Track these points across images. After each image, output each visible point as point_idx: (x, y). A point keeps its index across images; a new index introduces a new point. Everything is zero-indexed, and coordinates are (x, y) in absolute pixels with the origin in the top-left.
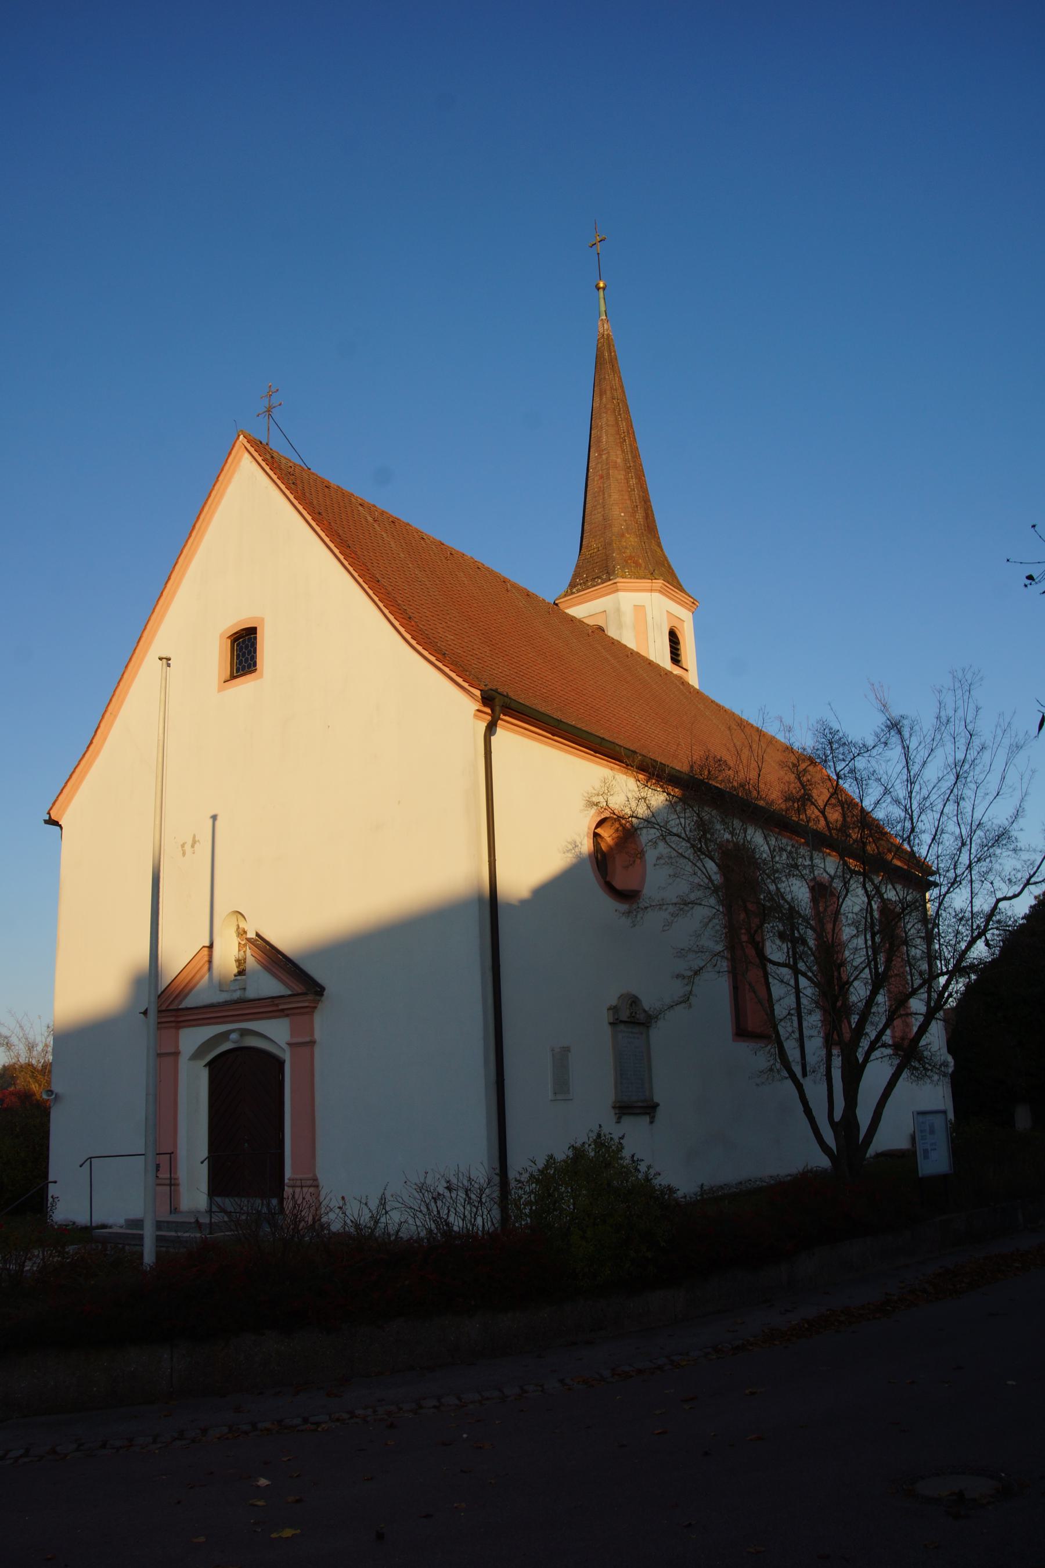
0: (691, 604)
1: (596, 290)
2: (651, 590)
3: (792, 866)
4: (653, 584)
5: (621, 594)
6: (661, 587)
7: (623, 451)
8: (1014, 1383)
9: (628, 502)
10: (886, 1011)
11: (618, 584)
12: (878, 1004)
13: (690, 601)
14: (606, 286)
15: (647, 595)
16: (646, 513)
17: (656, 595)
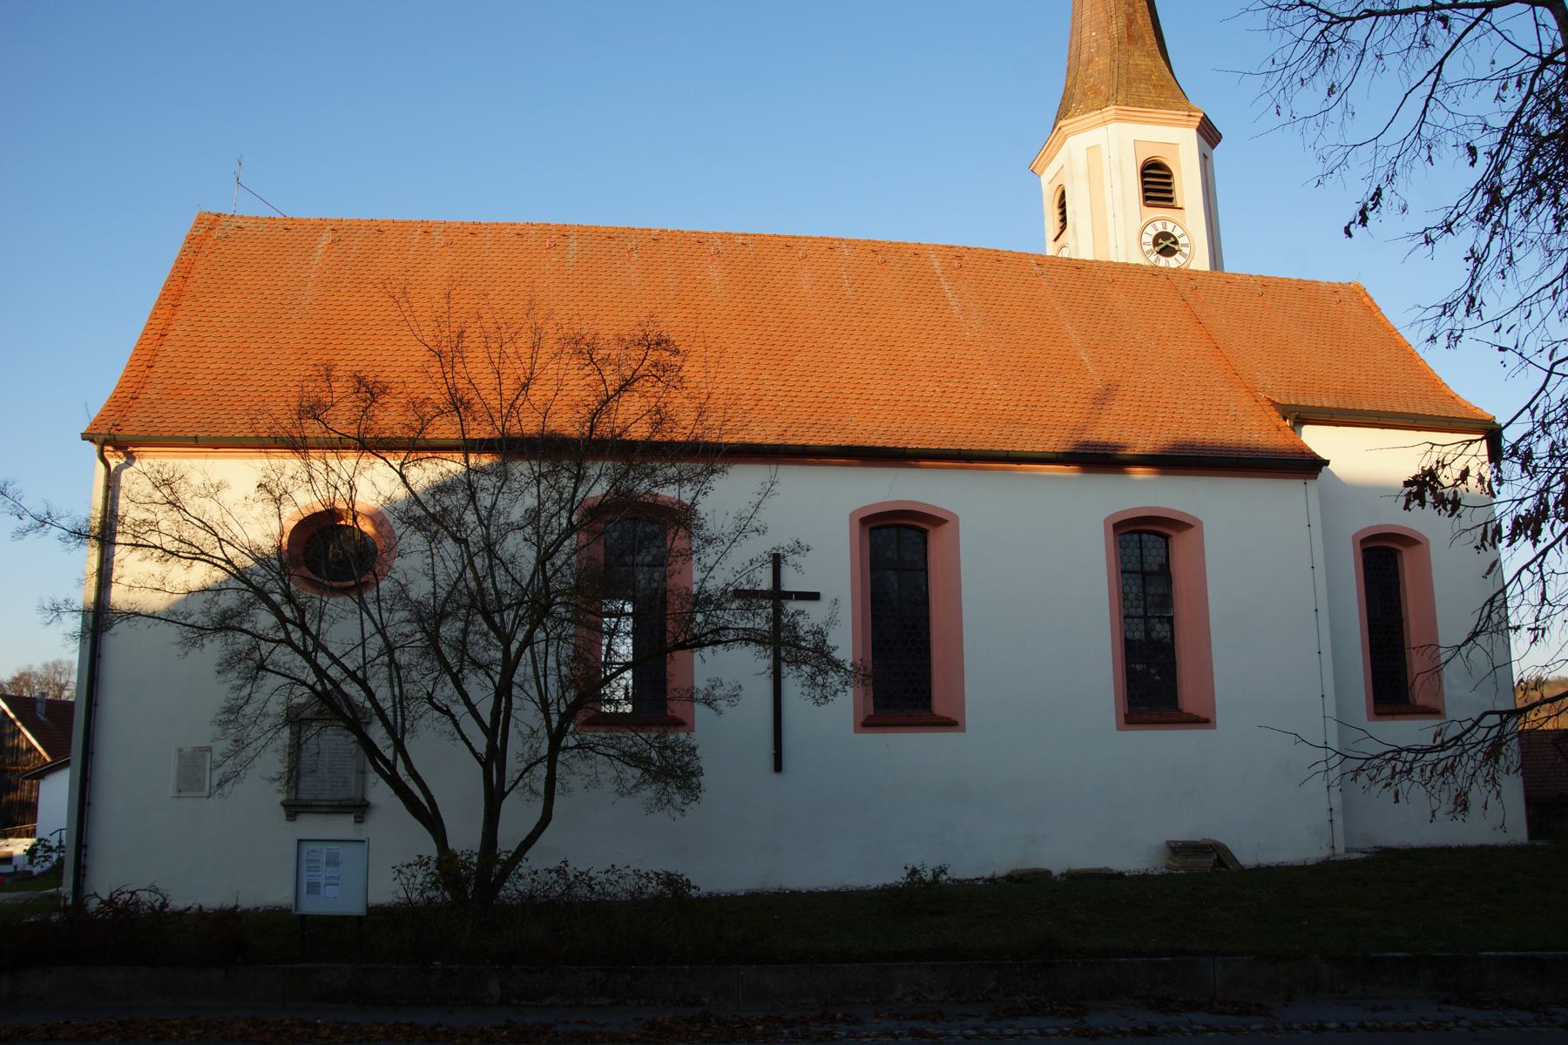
4: (1105, 114)
5: (1070, 140)
6: (1116, 114)
8: (389, 773)
10: (547, 884)
11: (1063, 129)
12: (660, 417)
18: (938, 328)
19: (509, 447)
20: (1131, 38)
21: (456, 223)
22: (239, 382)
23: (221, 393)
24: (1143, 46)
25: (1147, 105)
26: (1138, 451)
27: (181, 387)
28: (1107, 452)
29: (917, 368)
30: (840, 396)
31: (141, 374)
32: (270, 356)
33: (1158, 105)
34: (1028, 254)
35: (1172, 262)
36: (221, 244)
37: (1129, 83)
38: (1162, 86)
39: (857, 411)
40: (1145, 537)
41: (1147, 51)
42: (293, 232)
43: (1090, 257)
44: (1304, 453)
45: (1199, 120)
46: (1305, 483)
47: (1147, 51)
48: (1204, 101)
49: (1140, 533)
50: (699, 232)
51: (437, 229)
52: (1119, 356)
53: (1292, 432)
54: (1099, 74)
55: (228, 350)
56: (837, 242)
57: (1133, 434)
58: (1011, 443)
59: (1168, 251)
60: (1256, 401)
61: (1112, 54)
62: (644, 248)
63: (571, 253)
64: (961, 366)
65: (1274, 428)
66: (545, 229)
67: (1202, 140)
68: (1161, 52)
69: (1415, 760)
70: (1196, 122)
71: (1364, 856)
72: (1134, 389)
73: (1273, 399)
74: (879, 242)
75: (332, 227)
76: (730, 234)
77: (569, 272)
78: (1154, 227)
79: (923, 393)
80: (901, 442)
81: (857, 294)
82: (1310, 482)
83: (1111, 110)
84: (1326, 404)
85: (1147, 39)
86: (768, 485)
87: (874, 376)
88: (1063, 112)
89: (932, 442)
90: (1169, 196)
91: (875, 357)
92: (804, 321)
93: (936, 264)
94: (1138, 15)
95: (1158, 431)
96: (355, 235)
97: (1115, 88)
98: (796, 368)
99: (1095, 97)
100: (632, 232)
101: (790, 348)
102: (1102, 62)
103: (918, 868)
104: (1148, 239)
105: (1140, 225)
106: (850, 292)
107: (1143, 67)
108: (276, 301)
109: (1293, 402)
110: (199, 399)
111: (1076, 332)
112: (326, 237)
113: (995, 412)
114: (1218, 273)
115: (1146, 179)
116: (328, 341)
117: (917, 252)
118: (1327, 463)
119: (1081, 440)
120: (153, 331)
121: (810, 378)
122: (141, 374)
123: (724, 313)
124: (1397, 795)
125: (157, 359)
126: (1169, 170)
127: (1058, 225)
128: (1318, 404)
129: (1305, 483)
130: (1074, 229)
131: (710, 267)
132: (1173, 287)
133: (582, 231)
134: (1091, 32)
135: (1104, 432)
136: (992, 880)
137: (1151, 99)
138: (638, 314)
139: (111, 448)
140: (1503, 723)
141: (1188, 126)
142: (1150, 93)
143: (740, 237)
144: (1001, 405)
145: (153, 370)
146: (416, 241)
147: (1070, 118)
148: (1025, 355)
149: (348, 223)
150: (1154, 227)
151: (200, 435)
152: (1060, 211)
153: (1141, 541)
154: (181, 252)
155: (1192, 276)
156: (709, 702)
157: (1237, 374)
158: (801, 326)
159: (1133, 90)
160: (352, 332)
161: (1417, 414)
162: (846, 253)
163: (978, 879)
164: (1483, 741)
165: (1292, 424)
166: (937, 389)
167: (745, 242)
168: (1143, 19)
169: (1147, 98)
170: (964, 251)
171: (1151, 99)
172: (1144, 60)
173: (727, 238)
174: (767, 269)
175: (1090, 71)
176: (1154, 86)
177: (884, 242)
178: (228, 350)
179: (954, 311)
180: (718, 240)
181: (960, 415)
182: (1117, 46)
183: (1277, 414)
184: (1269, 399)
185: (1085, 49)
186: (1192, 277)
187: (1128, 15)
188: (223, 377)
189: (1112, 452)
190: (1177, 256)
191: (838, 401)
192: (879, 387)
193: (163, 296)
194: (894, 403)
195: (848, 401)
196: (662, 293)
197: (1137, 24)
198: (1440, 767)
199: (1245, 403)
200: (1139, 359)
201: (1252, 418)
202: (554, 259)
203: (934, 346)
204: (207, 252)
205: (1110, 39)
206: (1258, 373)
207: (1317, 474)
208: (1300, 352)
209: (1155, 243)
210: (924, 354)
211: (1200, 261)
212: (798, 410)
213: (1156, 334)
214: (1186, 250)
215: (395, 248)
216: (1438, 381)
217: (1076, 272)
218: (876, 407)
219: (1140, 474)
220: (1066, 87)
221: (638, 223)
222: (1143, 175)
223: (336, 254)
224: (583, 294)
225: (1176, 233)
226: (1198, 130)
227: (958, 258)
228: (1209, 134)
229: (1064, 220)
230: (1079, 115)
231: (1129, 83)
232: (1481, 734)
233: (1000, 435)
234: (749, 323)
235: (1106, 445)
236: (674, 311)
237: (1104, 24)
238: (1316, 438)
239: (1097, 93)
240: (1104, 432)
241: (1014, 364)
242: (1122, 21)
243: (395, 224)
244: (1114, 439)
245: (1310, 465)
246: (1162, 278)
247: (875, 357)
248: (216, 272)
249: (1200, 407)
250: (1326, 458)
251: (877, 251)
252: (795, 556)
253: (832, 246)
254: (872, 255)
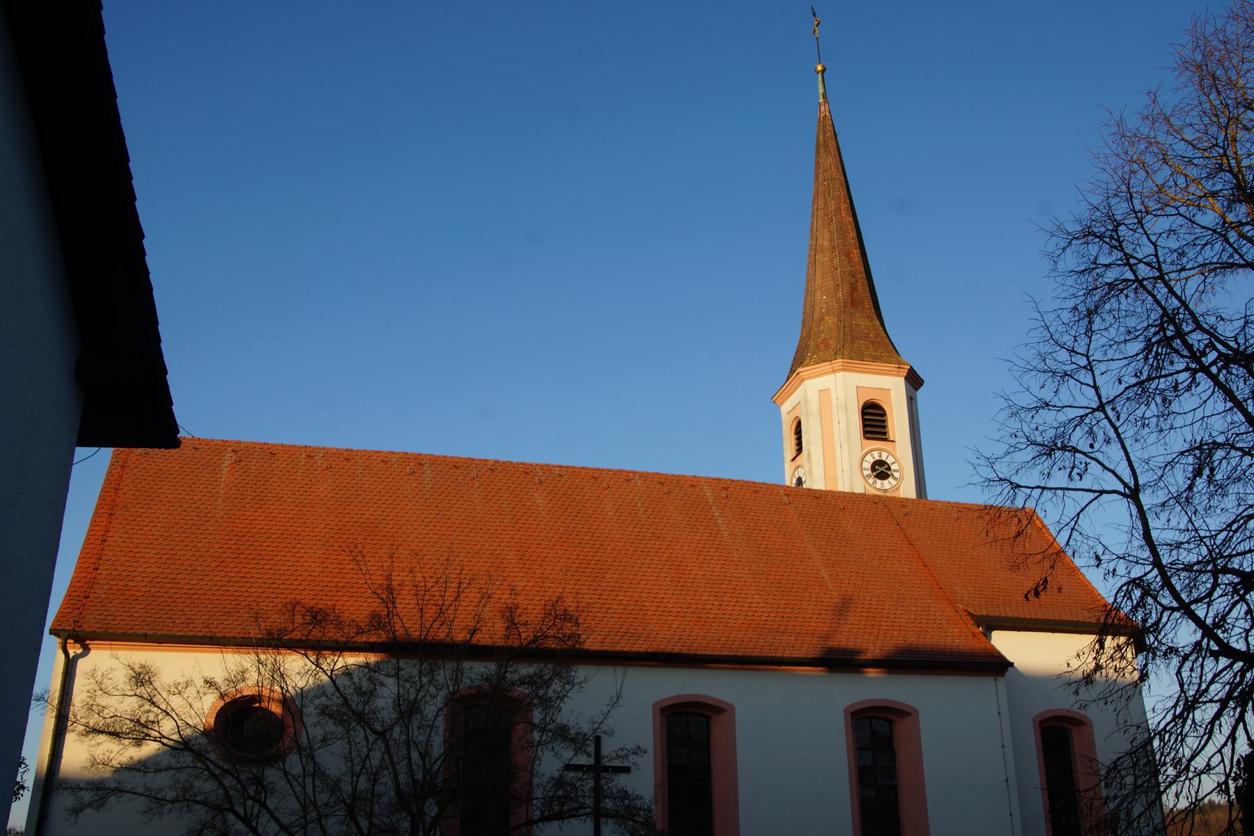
0: (896, 369)
1: (815, 73)
2: (834, 371)
3: (1143, 303)
4: (834, 365)
5: (806, 383)
6: (843, 365)
11: (801, 374)
13: (895, 367)
17: (840, 375)
19: (396, 648)
20: (853, 302)
21: (333, 449)
22: (172, 585)
23: (158, 595)
25: (866, 359)
27: (123, 588)
28: (847, 657)
29: (699, 584)
31: (89, 576)
32: (194, 563)
34: (778, 486)
36: (142, 460)
37: (852, 340)
39: (656, 622)
40: (874, 721)
41: (866, 314)
42: (201, 451)
44: (994, 656)
45: (907, 371)
46: (996, 680)
47: (866, 314)
48: (912, 356)
50: (525, 464)
51: (318, 454)
54: (828, 331)
55: (158, 556)
56: (631, 475)
57: (864, 641)
58: (774, 650)
59: (883, 476)
60: (957, 611)
64: (733, 583)
65: (970, 635)
66: (405, 457)
67: (909, 385)
73: (968, 610)
74: (664, 475)
75: (232, 448)
76: (549, 466)
77: (427, 496)
78: (872, 455)
79: (705, 606)
82: (1000, 680)
84: (1010, 614)
85: (866, 303)
86: (615, 699)
88: (799, 360)
89: (715, 649)
90: (883, 424)
94: (859, 284)
95: (883, 637)
96: (252, 457)
97: (841, 343)
98: (607, 584)
99: (826, 349)
102: (830, 321)
104: (867, 465)
107: (863, 327)
108: (194, 514)
109: (984, 613)
110: (140, 599)
111: (817, 553)
112: (228, 459)
115: (865, 417)
116: (240, 551)
117: (693, 484)
120: (95, 537)
121: (618, 593)
122: (89, 576)
125: (101, 562)
126: (884, 410)
127: (794, 448)
128: (1003, 615)
129: (996, 680)
130: (809, 454)
131: (535, 494)
132: (889, 514)
134: (822, 296)
135: (843, 640)
137: (869, 353)
139: (72, 641)
141: (898, 376)
142: (869, 348)
143: (557, 469)
144: (764, 616)
145: (99, 572)
146: (302, 463)
147: (807, 366)
149: (245, 445)
150: (872, 455)
151: (148, 632)
153: (871, 724)
154: (110, 466)
155: (904, 502)
157: (941, 589)
159: (856, 345)
160: (258, 543)
161: (1079, 621)
162: (639, 484)
165: (984, 630)
166: (715, 603)
167: (561, 473)
168: (862, 288)
169: (866, 352)
170: (729, 483)
171: (869, 353)
172: (864, 322)
173: (547, 469)
174: (579, 497)
175: (821, 328)
177: (668, 475)
178: (158, 556)
179: (724, 536)
180: (540, 471)
181: (734, 625)
182: (842, 309)
183: (972, 622)
184: (966, 610)
185: (817, 309)
186: (904, 504)
187: (851, 284)
188: (158, 580)
193: (99, 506)
194: (683, 615)
195: (649, 613)
196: (500, 517)
199: (948, 613)
200: (866, 576)
202: (414, 485)
203: (711, 566)
204: (131, 467)
205: (837, 303)
206: (956, 587)
207: (1005, 672)
208: (988, 568)
209: (873, 469)
211: (908, 490)
214: (897, 475)
215: (285, 470)
217: (815, 501)
219: (872, 673)
221: (477, 454)
223: (238, 473)
224: (439, 516)
225: (890, 461)
226: (906, 378)
227: (725, 488)
228: (914, 381)
230: (813, 364)
231: (852, 340)
233: (765, 642)
234: (569, 544)
237: (832, 290)
238: (1006, 643)
239: (827, 346)
240: (844, 639)
242: (846, 288)
243: (283, 448)
244: (851, 645)
245: (998, 665)
246: (881, 506)
248: (141, 485)
249: (913, 616)
251: (666, 485)
253: (628, 478)
254: (659, 486)
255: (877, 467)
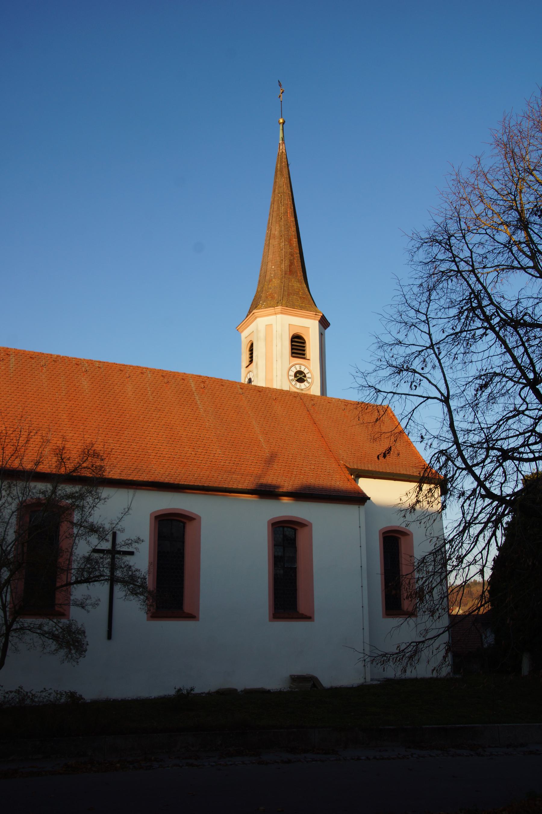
0: (314, 315)
2: (276, 314)
4: (276, 310)
6: (281, 311)
7: (280, 226)
9: (278, 258)
11: (255, 314)
14: (285, 121)
15: (274, 317)
16: (290, 263)
17: (279, 316)
18: (193, 420)
20: (291, 271)
24: (297, 276)
26: (285, 490)
30: (147, 454)
33: (301, 308)
35: (303, 386)
37: (288, 295)
38: (304, 298)
40: (285, 529)
43: (264, 385)
44: (359, 493)
45: (320, 317)
49: (283, 527)
52: (277, 439)
53: (354, 482)
56: (145, 370)
60: (339, 465)
61: (281, 279)
62: (49, 365)
63: (11, 364)
65: (346, 480)
67: (321, 327)
68: (305, 281)
69: (390, 656)
70: (319, 318)
71: (379, 682)
72: (283, 457)
73: (346, 465)
74: (165, 371)
77: (11, 376)
78: (295, 367)
80: (176, 480)
81: (155, 399)
83: (279, 308)
84: (370, 469)
86: (127, 510)
87: (163, 444)
88: (255, 305)
90: (303, 353)
91: (163, 434)
92: (129, 412)
93: (193, 385)
95: (294, 479)
97: (282, 296)
100: (43, 355)
101: (122, 427)
102: (276, 282)
103: (182, 688)
104: (292, 373)
105: (289, 366)
106: (151, 398)
109: (355, 467)
113: (219, 466)
114: (324, 397)
115: (293, 344)
118: (369, 498)
119: (259, 483)
121: (132, 443)
123: (90, 405)
124: (384, 669)
128: (367, 469)
130: (257, 364)
131: (82, 378)
133: (17, 353)
136: (209, 694)
137: (298, 304)
138: (47, 402)
140: (417, 645)
141: (315, 319)
142: (298, 301)
143: (97, 363)
148: (233, 436)
150: (295, 367)
152: (250, 353)
155: (312, 398)
156: (82, 606)
158: (128, 415)
159: (290, 298)
163: (202, 693)
164: (410, 651)
166: (193, 453)
167: (100, 366)
171: (298, 304)
172: (296, 285)
173: (91, 362)
175: (270, 286)
176: (300, 297)
177: (168, 371)
180: (86, 364)
182: (284, 275)
184: (345, 465)
185: (268, 273)
186: (312, 398)
187: (290, 260)
189: (273, 490)
190: (305, 383)
191: (146, 456)
192: (165, 450)
195: (151, 457)
197: (294, 265)
198: (398, 659)
201: (337, 474)
206: (340, 451)
209: (295, 376)
210: (186, 434)
211: (316, 390)
212: (127, 460)
213: (295, 428)
214: (309, 380)
216: (421, 458)
217: (259, 393)
218: (164, 461)
219: (286, 500)
220: (257, 291)
222: (292, 341)
225: (306, 371)
226: (319, 322)
228: (324, 323)
229: (251, 357)
230: (263, 308)
232: (410, 649)
235: (270, 486)
236: (66, 402)
237: (279, 263)
239: (273, 298)
240: (270, 479)
241: (229, 441)
242: (287, 263)
244: (274, 482)
246: (298, 399)
247: (163, 434)
249: (313, 467)
250: (369, 497)
252: (136, 544)
254: (162, 378)
255: (298, 375)
